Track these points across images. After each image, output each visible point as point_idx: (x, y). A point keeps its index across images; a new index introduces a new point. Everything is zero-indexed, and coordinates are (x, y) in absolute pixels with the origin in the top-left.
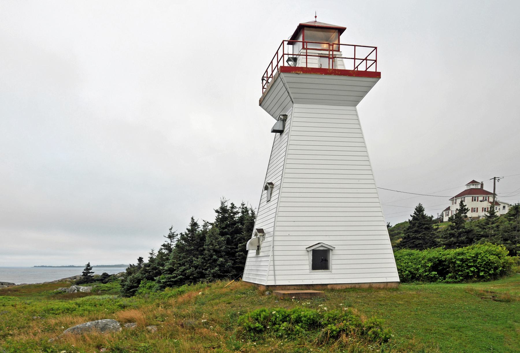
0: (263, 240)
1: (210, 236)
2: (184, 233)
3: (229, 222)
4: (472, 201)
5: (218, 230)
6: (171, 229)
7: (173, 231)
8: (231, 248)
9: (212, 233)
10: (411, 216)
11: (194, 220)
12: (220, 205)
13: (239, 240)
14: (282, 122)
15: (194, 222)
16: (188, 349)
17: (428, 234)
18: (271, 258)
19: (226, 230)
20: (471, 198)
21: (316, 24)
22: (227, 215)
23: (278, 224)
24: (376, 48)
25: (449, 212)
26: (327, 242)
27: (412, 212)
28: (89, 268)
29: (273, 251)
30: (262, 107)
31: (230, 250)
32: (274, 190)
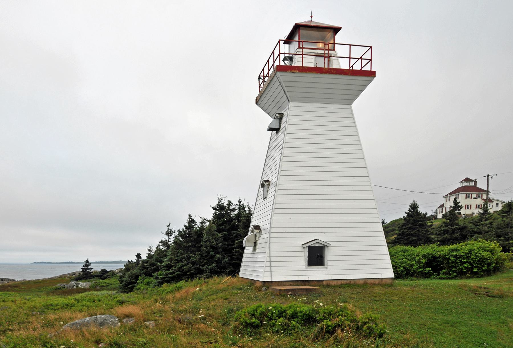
0: (259, 237)
1: (207, 233)
2: (181, 230)
3: (226, 219)
4: (466, 198)
5: (215, 227)
6: (168, 226)
7: (170, 228)
8: (227, 245)
9: (209, 230)
10: (405, 213)
11: (191, 217)
12: (217, 202)
13: (236, 236)
14: (278, 120)
15: (191, 219)
16: (186, 344)
17: (423, 231)
18: (267, 254)
19: (223, 227)
20: (465, 195)
21: (312, 24)
22: (224, 212)
23: (274, 221)
24: (371, 47)
25: (443, 209)
26: (323, 238)
27: (407, 209)
28: (88, 264)
29: (270, 247)
30: (259, 106)
31: (227, 246)
32: (270, 187)
